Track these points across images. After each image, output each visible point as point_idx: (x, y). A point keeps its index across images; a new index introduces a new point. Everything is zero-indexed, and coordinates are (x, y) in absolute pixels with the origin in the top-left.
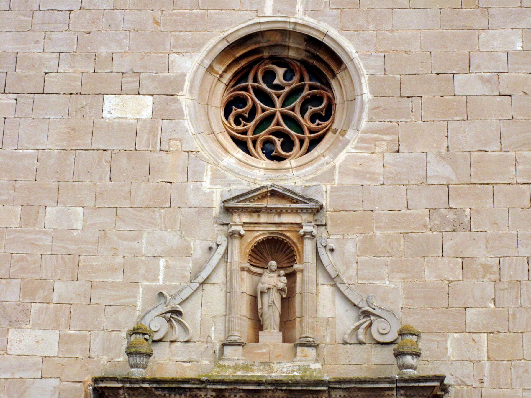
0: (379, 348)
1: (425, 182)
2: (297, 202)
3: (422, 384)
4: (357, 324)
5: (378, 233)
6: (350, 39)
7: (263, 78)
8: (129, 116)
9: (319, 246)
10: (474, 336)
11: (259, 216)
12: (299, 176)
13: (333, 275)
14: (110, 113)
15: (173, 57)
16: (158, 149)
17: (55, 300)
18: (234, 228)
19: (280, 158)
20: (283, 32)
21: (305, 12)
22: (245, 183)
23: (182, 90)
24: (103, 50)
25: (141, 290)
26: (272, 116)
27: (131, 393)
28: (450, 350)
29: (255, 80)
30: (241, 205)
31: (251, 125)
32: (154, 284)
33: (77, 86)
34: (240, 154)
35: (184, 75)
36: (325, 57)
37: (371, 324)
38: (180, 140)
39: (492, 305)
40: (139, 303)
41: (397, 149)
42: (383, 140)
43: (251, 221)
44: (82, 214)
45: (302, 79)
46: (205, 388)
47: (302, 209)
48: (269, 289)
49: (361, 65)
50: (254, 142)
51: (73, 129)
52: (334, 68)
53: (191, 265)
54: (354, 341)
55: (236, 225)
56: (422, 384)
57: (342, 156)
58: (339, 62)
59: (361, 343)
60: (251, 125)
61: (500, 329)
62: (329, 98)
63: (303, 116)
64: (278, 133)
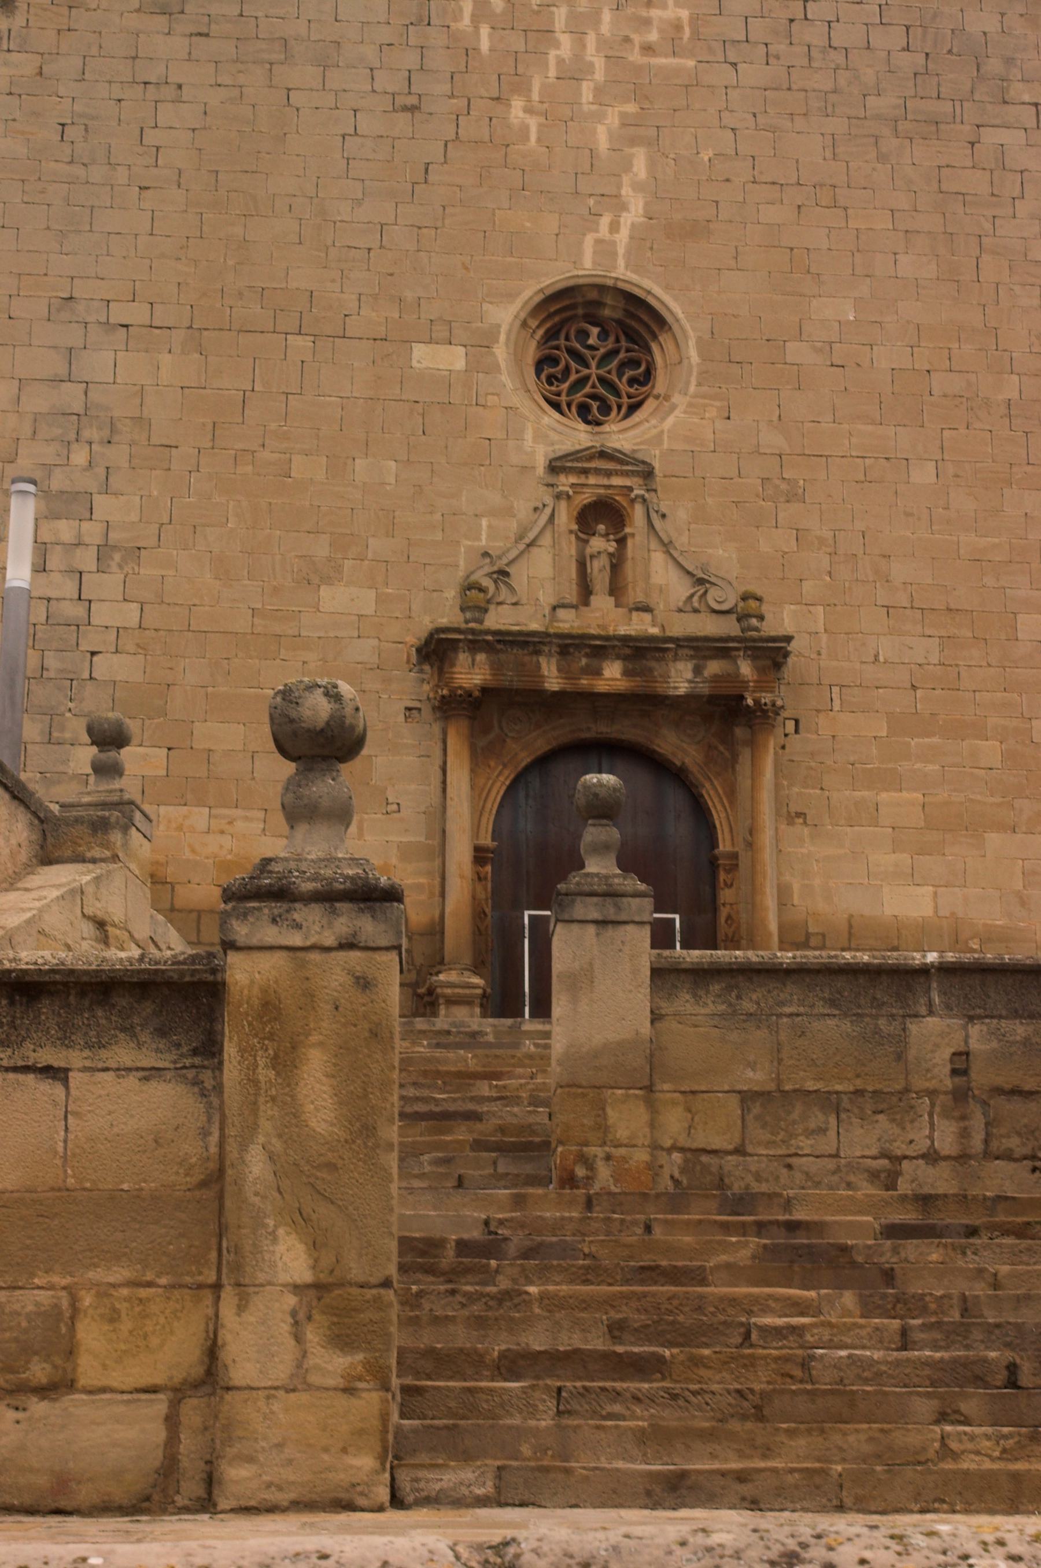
0: (714, 615)
1: (757, 452)
2: (627, 464)
3: (770, 645)
4: (692, 591)
5: (709, 500)
6: (676, 299)
7: (576, 337)
8: (441, 367)
9: (651, 510)
10: (811, 608)
11: (587, 477)
12: (625, 439)
13: (666, 541)
14: (419, 362)
15: (485, 306)
16: (474, 403)
17: (370, 556)
18: (561, 488)
19: (598, 424)
20: (602, 288)
21: (626, 268)
22: (569, 443)
23: (498, 342)
24: (409, 295)
25: (463, 549)
26: (587, 378)
27: (471, 646)
28: (786, 621)
29: (567, 339)
30: (569, 464)
31: (565, 386)
32: (476, 543)
33: (382, 331)
34: (556, 415)
35: (499, 326)
36: (645, 317)
37: (706, 592)
38: (498, 395)
39: (828, 579)
40: (462, 563)
41: (727, 415)
42: (712, 406)
43: (579, 482)
44: (394, 468)
45: (618, 341)
46: (550, 643)
47: (632, 472)
48: (599, 553)
49: (688, 327)
50: (569, 405)
51: (380, 378)
52: (655, 328)
53: (515, 525)
54: (688, 608)
55: (563, 485)
56: (770, 645)
57: (670, 420)
58: (661, 322)
59: (696, 611)
60: (565, 386)
61: (836, 602)
62: (648, 362)
63: (620, 380)
64: (594, 397)
